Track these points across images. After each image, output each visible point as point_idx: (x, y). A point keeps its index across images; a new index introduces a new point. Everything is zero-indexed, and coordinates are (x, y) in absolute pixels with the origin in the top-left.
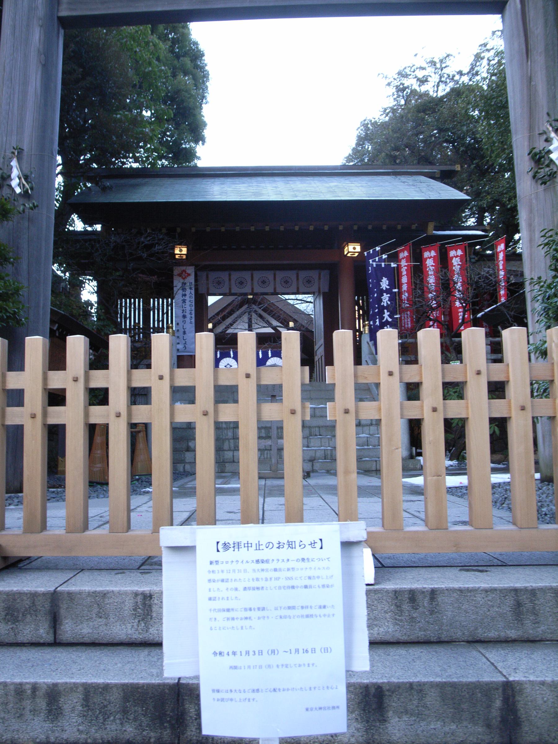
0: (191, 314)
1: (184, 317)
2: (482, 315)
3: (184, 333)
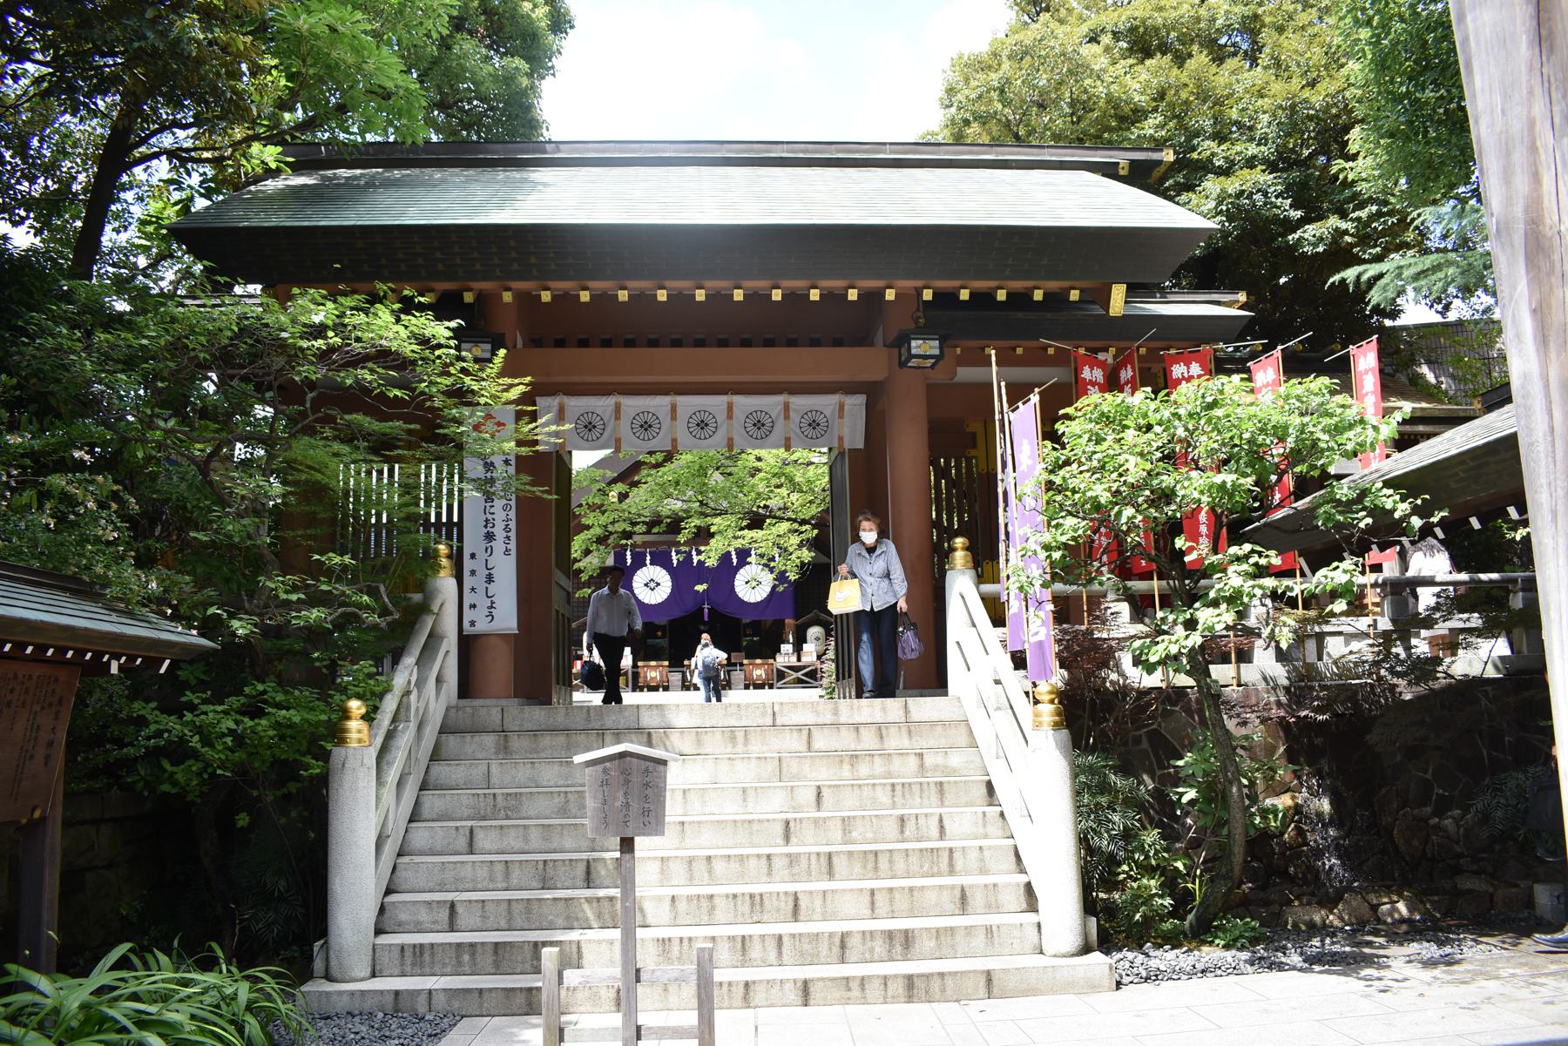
0: (507, 529)
1: (490, 537)
2: (1491, 581)
3: (490, 579)
